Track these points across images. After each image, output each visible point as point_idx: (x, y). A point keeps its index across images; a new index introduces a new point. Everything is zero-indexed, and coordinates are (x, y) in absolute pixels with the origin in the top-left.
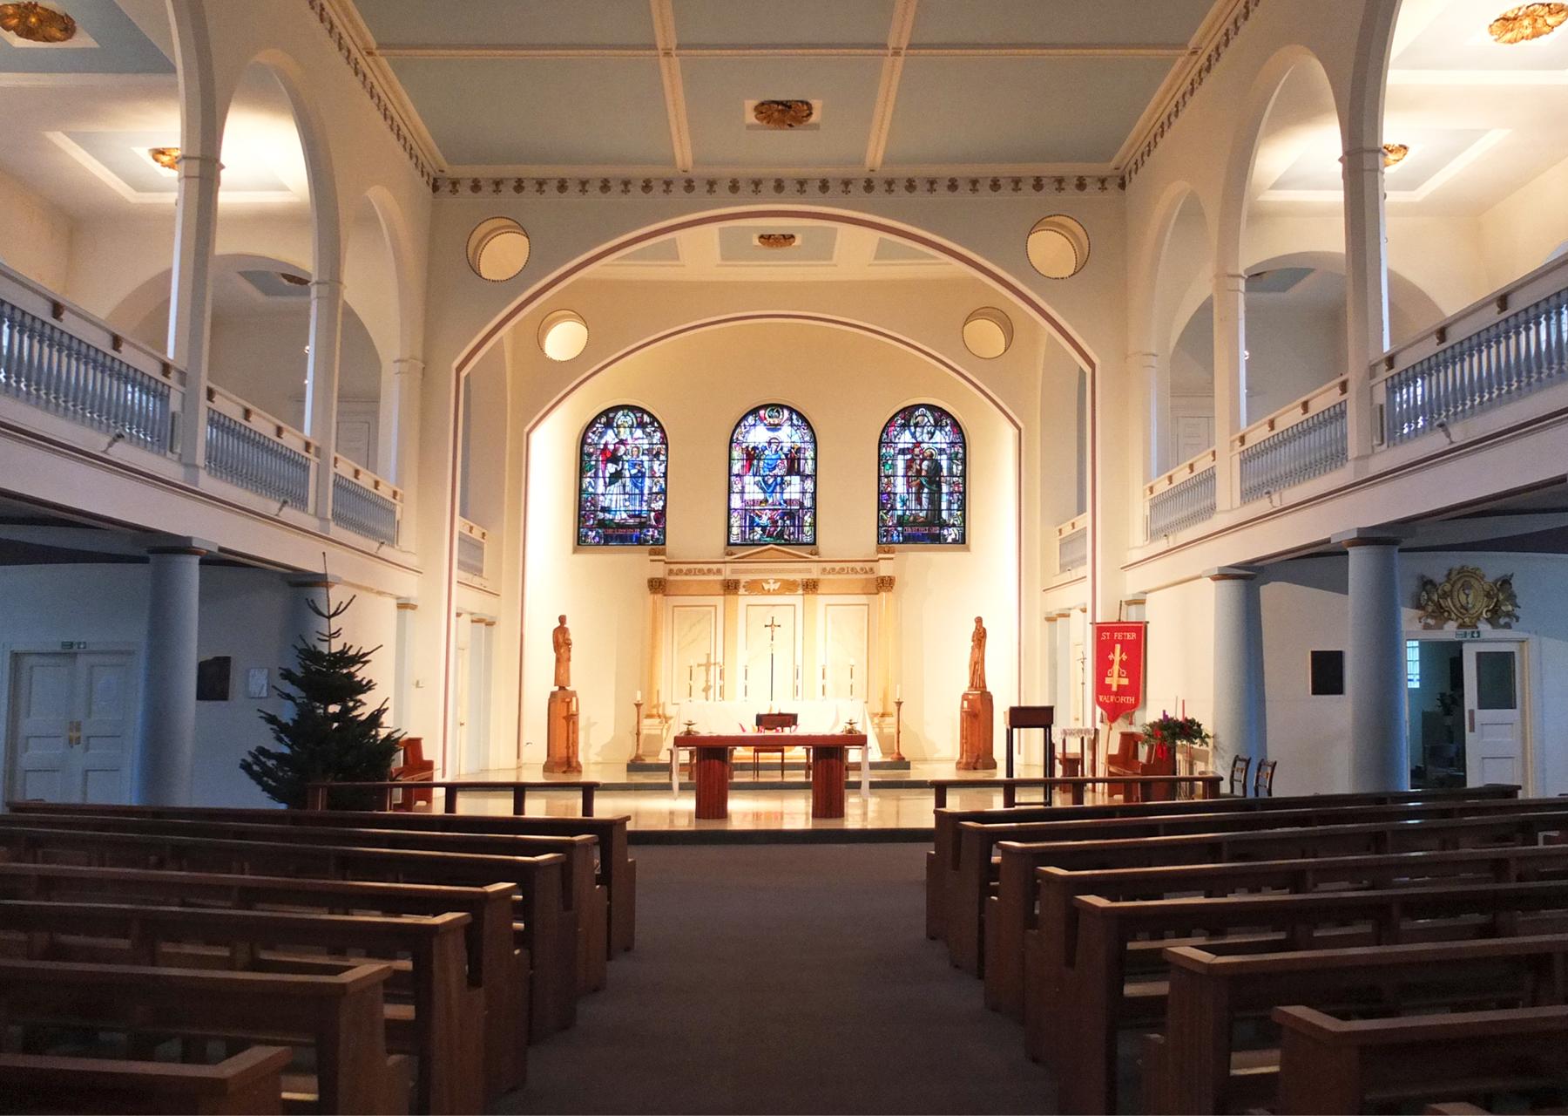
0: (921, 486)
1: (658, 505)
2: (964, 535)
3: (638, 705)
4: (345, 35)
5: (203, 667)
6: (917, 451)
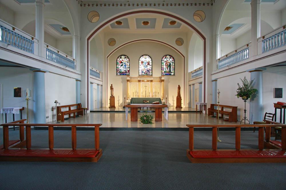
0: (168, 67)
1: (128, 69)
2: (174, 74)
3: (125, 98)
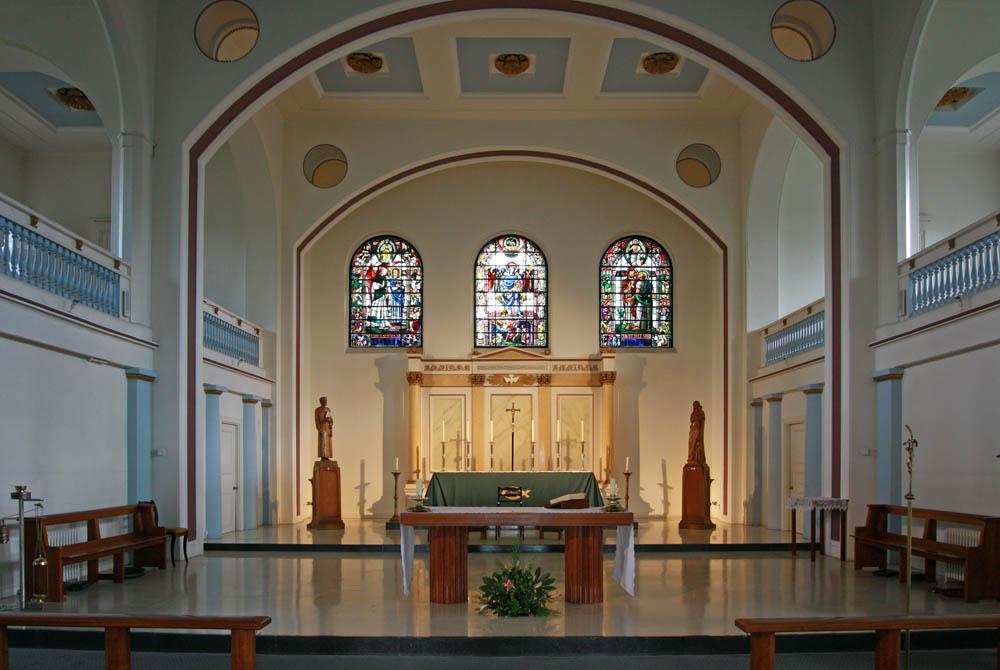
6: (631, 273)
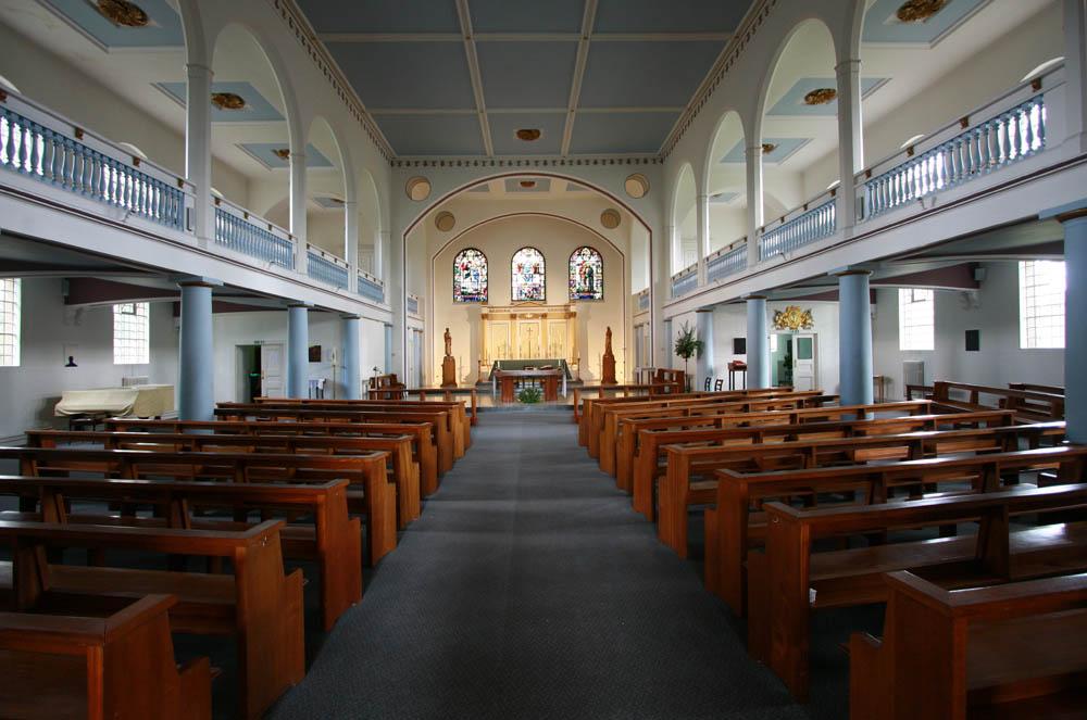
1: (485, 286)
4: (286, 10)
5: (311, 350)
